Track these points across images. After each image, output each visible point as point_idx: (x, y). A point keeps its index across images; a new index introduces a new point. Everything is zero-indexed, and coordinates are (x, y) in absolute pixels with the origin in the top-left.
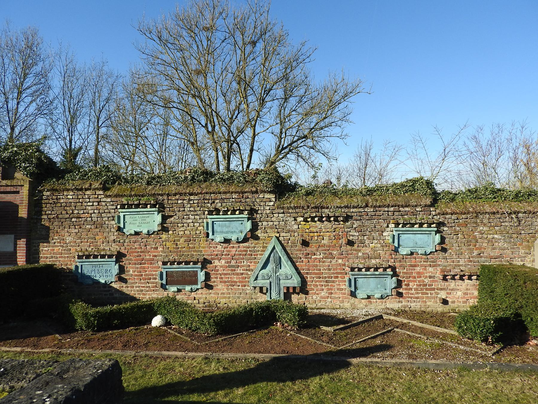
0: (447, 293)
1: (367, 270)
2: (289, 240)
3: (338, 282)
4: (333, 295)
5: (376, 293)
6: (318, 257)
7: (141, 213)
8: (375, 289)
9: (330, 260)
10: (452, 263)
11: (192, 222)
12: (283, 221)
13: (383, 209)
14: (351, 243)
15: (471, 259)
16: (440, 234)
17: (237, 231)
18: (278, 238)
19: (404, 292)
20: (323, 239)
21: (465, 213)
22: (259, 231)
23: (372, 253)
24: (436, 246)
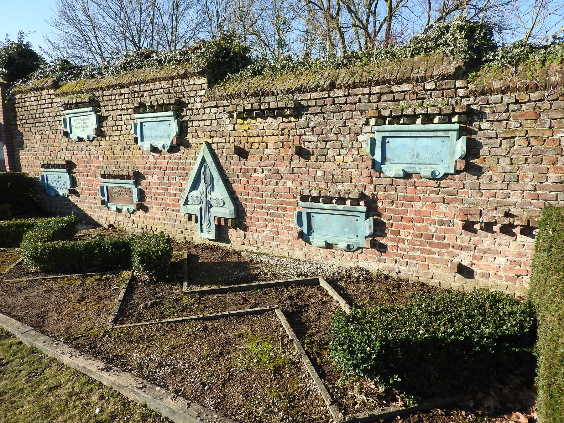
0: (474, 257)
1: (327, 201)
2: (224, 148)
4: (279, 236)
5: (341, 241)
6: (260, 176)
7: (81, 114)
9: (275, 181)
10: (491, 199)
11: (125, 125)
12: (216, 119)
13: (360, 91)
14: (303, 153)
15: (539, 192)
17: (165, 136)
18: (209, 145)
19: (389, 244)
20: (267, 148)
21: (537, 88)
22: (189, 136)
23: (339, 172)
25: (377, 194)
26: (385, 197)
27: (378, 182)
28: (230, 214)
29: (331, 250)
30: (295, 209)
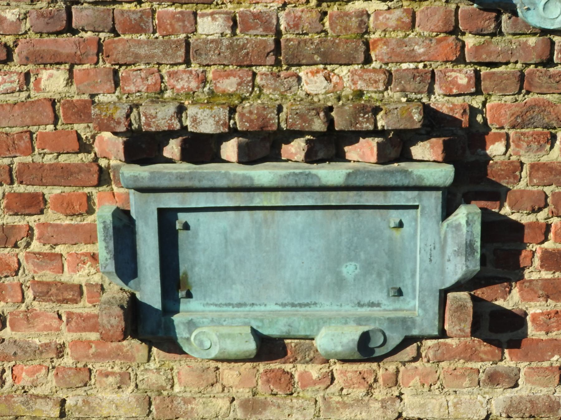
3: (44, 241)
5: (326, 320)
8: (317, 288)
25: (484, 104)
26: (521, 115)
27: (489, 54)
28: (408, 18)
29: (275, 365)
30: (89, 198)
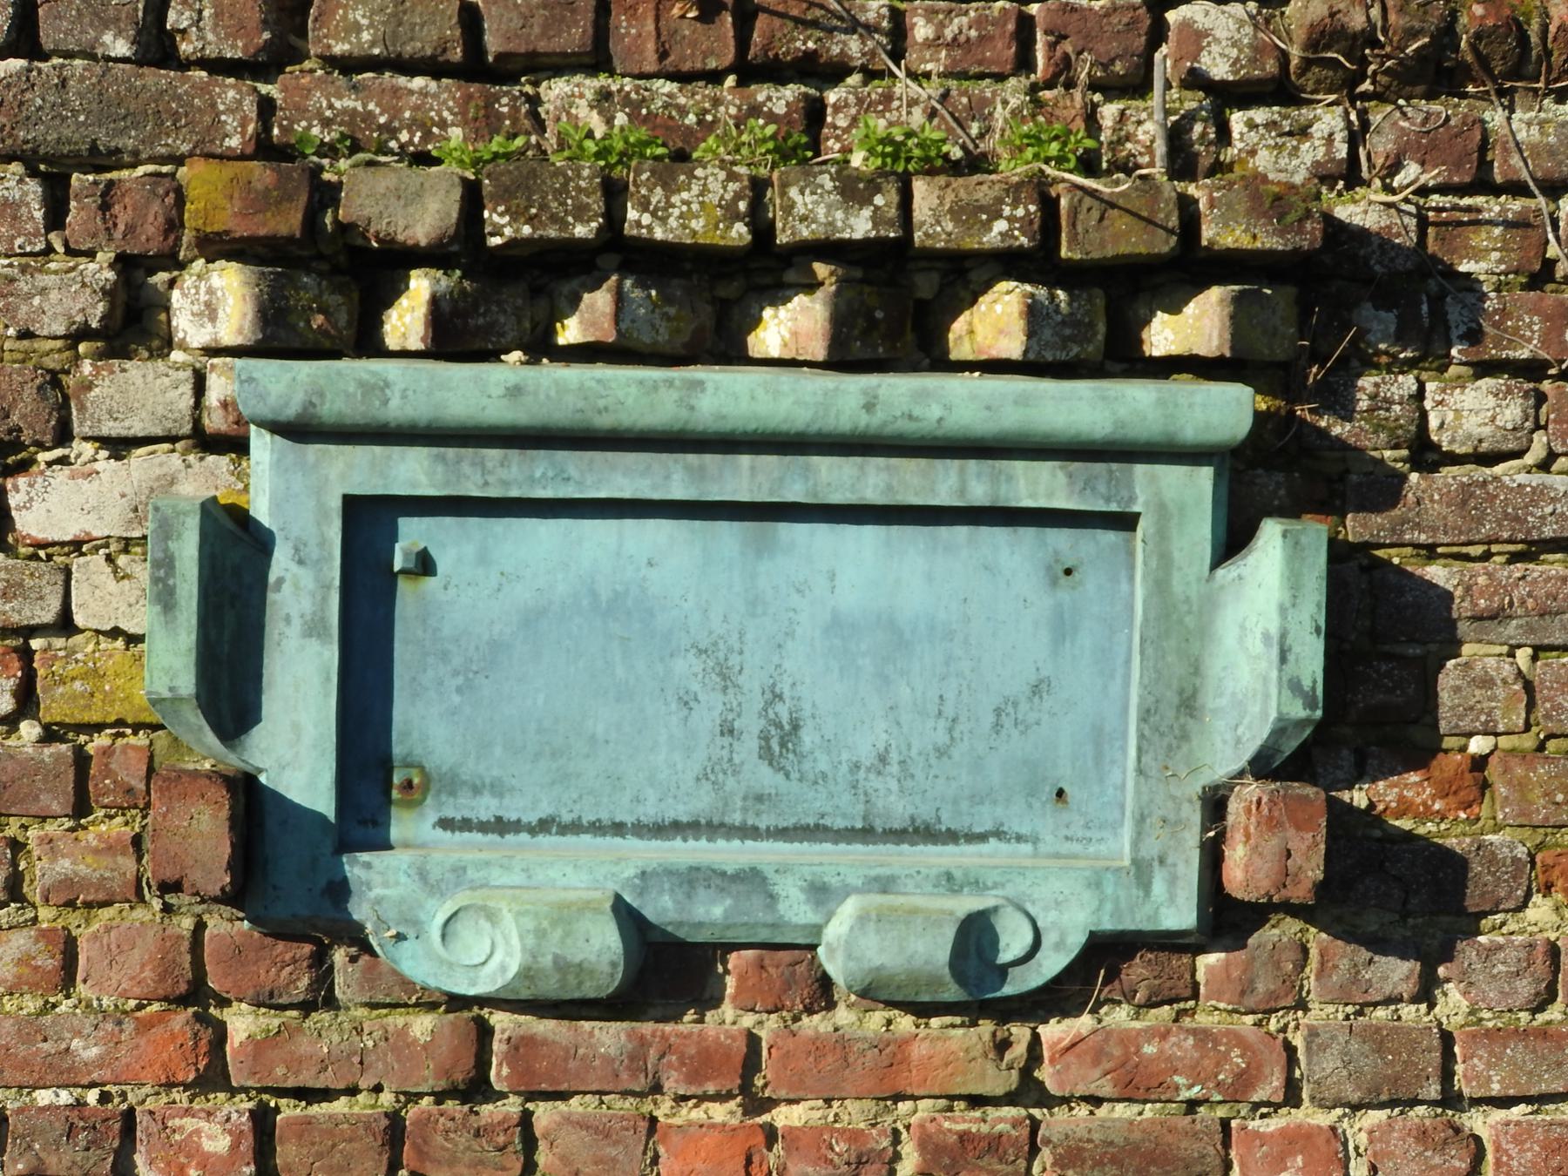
16: (1315, 532)
24: (1215, 804)
